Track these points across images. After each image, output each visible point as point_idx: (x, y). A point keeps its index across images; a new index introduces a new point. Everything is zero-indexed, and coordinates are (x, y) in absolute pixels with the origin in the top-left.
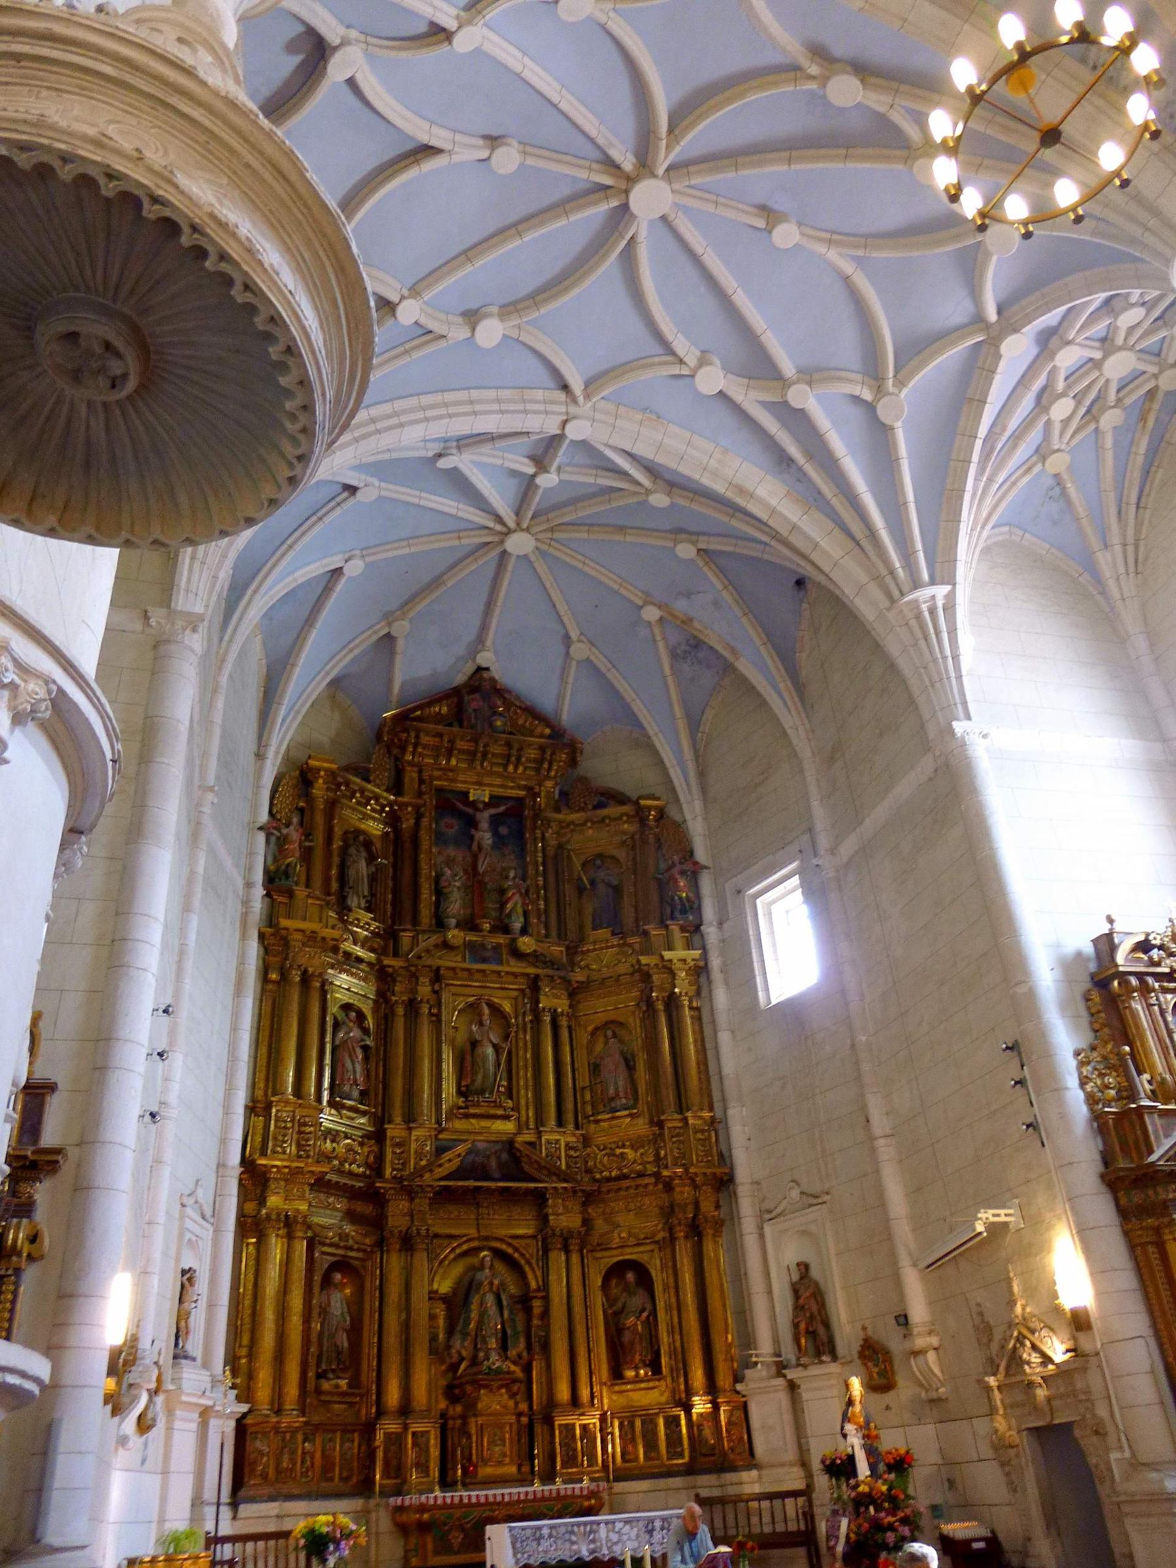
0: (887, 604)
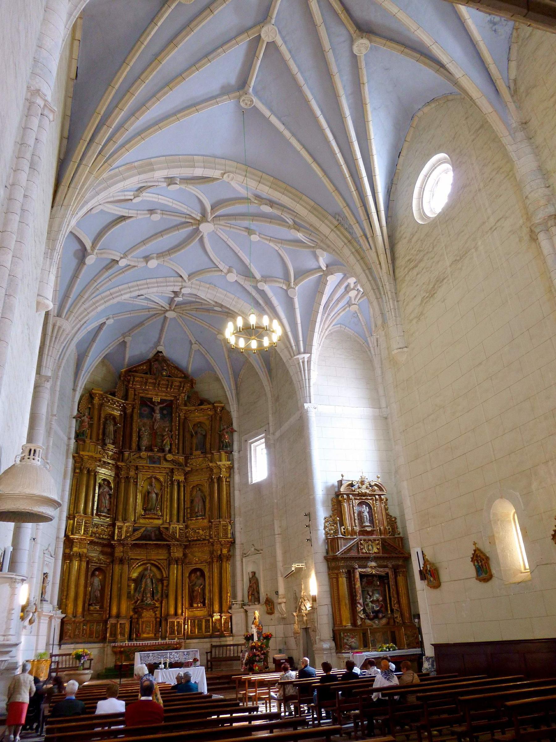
0: (290, 357)
